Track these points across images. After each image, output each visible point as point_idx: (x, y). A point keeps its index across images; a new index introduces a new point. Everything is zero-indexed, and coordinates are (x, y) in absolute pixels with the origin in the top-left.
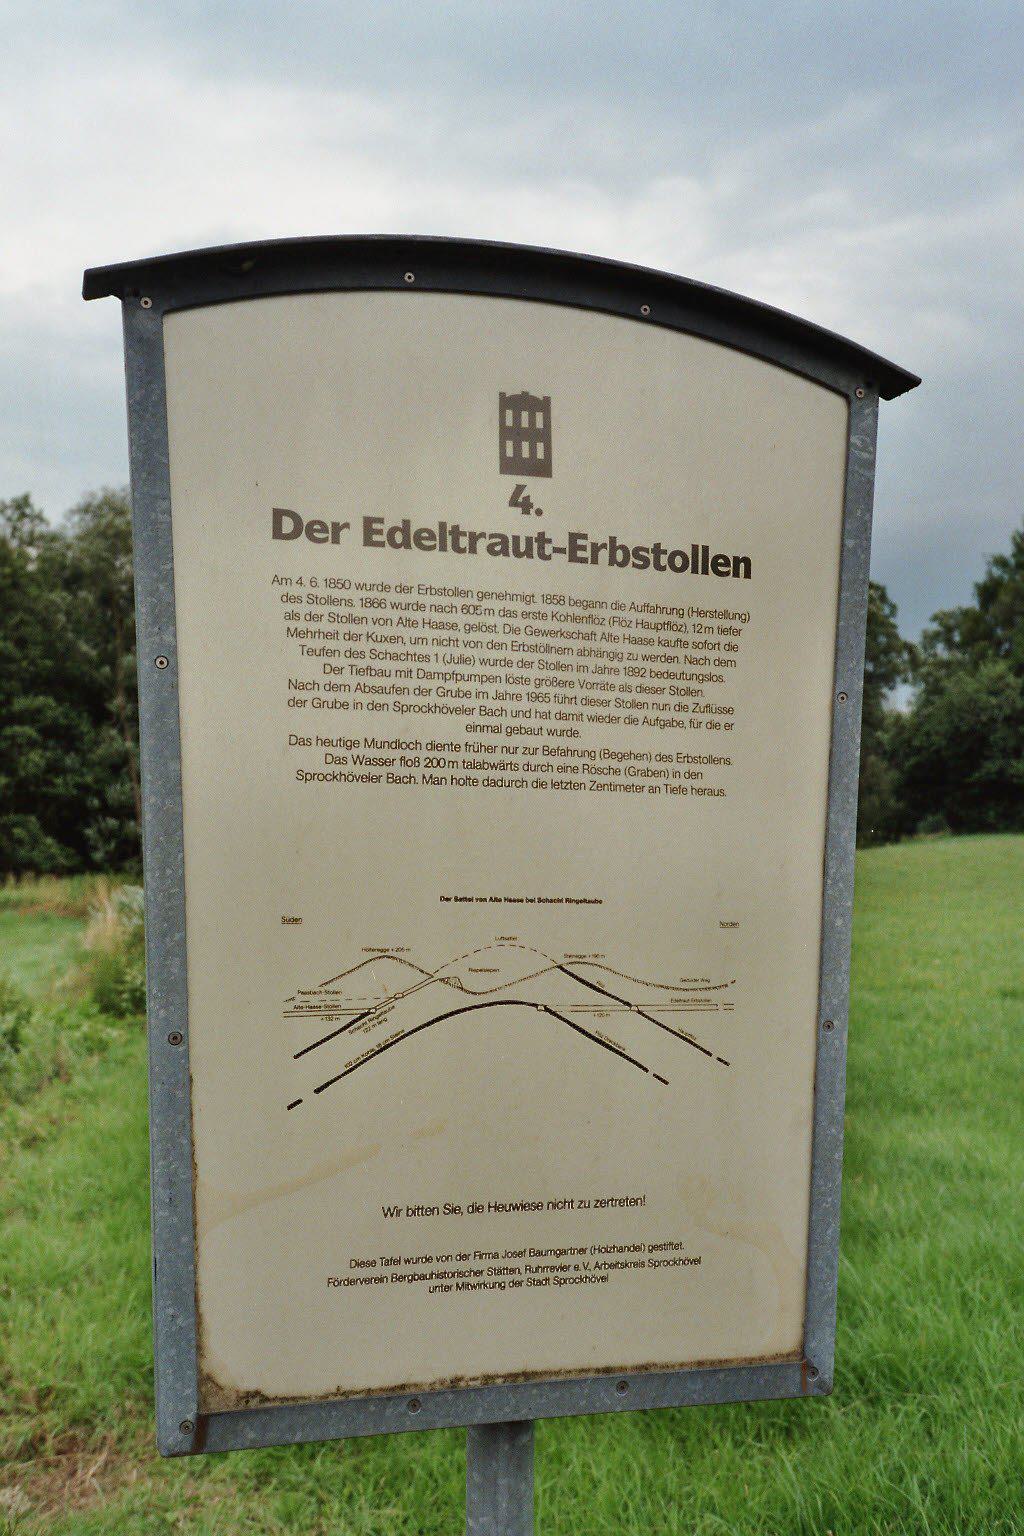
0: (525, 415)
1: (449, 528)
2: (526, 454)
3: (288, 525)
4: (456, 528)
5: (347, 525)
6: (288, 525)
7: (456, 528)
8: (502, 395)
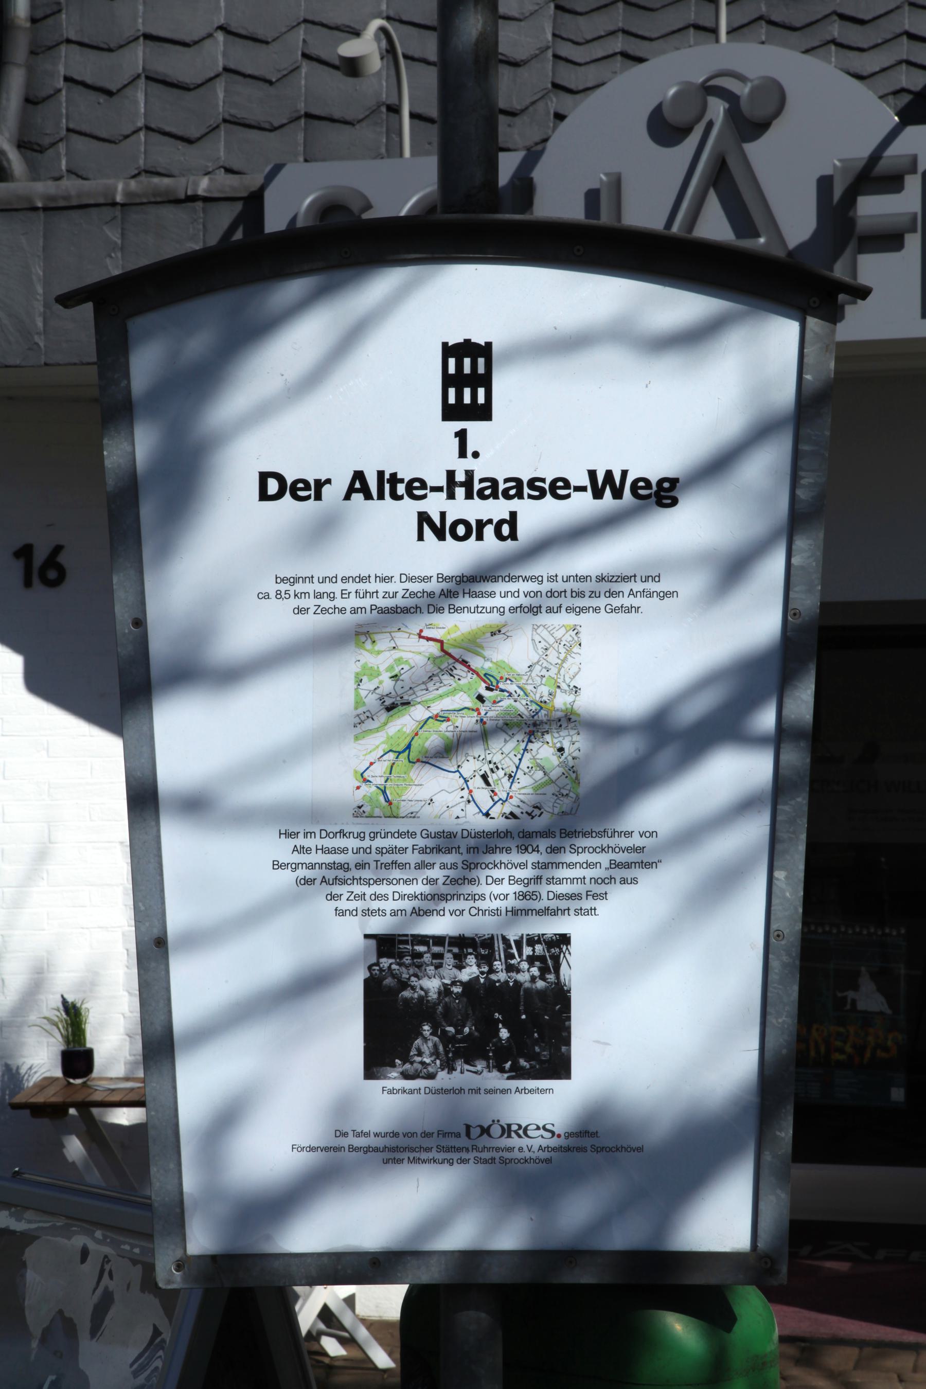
0: (467, 362)
1: (387, 476)
2: (467, 399)
3: (273, 486)
4: (394, 476)
5: (328, 481)
6: (273, 486)
7: (394, 476)
8: (445, 345)
